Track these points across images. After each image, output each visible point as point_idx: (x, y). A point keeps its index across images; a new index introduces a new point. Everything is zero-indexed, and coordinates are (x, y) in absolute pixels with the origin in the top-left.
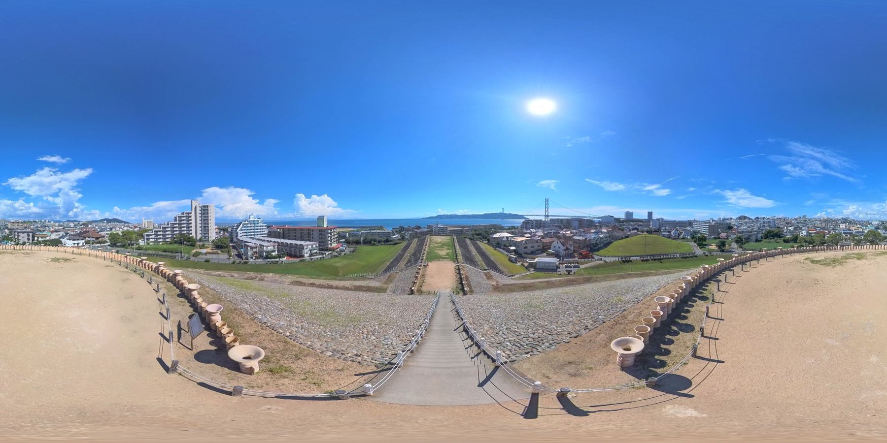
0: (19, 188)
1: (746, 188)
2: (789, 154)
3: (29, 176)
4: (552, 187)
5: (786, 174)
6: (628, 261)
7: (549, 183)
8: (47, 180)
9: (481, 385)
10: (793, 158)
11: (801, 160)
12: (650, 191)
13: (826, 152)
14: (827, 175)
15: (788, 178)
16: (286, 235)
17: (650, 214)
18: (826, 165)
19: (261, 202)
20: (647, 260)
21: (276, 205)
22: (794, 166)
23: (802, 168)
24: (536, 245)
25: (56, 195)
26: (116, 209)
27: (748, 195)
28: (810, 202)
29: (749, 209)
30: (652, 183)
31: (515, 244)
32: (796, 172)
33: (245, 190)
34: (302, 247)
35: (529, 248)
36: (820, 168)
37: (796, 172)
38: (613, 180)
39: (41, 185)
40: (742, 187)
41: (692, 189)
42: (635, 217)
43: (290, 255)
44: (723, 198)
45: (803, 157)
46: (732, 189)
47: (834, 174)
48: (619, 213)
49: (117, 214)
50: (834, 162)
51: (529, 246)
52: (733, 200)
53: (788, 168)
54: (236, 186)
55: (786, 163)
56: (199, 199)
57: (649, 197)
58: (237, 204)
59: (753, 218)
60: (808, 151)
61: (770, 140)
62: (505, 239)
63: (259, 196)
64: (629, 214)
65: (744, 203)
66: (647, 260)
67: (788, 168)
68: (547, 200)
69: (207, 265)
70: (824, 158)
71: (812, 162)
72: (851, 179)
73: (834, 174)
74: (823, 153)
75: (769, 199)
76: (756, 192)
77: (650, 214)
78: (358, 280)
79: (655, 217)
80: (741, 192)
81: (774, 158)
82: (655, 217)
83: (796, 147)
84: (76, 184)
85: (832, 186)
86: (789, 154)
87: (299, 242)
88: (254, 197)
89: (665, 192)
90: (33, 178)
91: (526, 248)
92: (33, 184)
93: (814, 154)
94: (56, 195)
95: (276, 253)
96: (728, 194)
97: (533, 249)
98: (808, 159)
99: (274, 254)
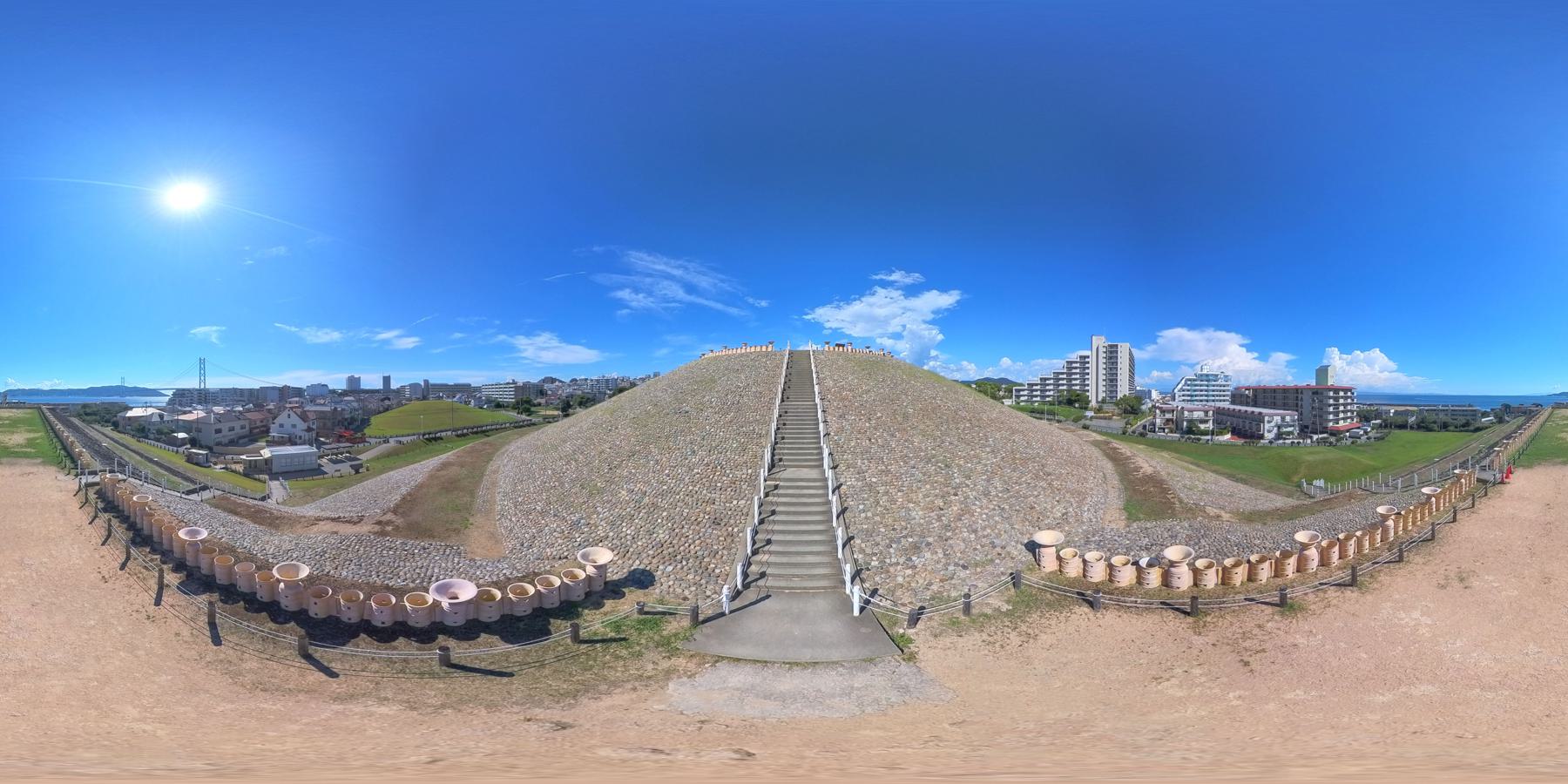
0: (834, 325)
1: (552, 330)
2: (627, 271)
3: (848, 301)
5: (622, 304)
6: (436, 439)
7: (209, 332)
8: (881, 312)
9: (123, 567)
11: (648, 280)
12: (386, 342)
13: (690, 266)
14: (691, 305)
15: (625, 311)
16: (1260, 399)
17: (387, 380)
18: (690, 289)
19: (1263, 357)
20: (464, 435)
22: (636, 290)
23: (650, 293)
24: (237, 425)
25: (897, 336)
26: (1006, 361)
27: (555, 343)
28: (664, 351)
29: (556, 366)
30: (389, 328)
31: (187, 426)
32: (639, 301)
33: (1233, 335)
34: (1260, 419)
35: (225, 432)
36: (681, 294)
37: (639, 301)
39: (871, 319)
40: (545, 330)
41: (458, 335)
42: (365, 385)
43: (1236, 432)
44: (512, 348)
45: (650, 275)
46: (529, 333)
47: (706, 302)
48: (337, 382)
49: (1006, 370)
50: (704, 282)
51: (225, 427)
52: (529, 352)
53: (625, 294)
54: (1219, 328)
55: (621, 287)
56: (1151, 348)
59: (567, 380)
62: (156, 419)
63: (1259, 346)
64: (353, 381)
65: (548, 356)
66: (464, 435)
67: (625, 294)
68: (202, 362)
69: (1161, 445)
71: (666, 283)
72: (734, 311)
73: (706, 302)
74: (686, 269)
75: (590, 347)
76: (568, 336)
77: (387, 380)
79: (394, 385)
80: (544, 339)
81: (601, 278)
82: (394, 385)
83: (639, 259)
84: (932, 316)
86: (627, 271)
87: (1257, 410)
88: (1249, 348)
89: (410, 342)
90: (857, 307)
91: (218, 431)
92: (858, 318)
93: (669, 270)
94: (897, 336)
95: (1210, 425)
96: (521, 341)
97: (232, 435)
98: (659, 278)
99: (1202, 427)
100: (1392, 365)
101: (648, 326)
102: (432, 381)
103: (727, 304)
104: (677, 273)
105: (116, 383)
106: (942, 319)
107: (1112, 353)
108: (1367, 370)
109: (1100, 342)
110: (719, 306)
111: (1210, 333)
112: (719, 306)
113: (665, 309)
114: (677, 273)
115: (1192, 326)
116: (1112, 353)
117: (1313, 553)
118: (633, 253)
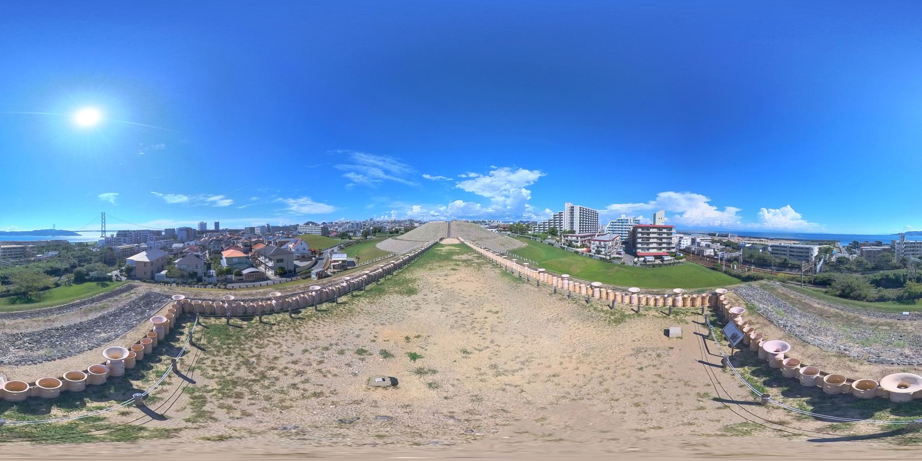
4: (112, 201)
5: (349, 181)
7: (109, 196)
10: (358, 167)
11: (365, 168)
12: (214, 202)
13: (388, 160)
14: (387, 181)
15: (351, 185)
17: (217, 224)
18: (387, 172)
19: (721, 209)
21: (737, 213)
22: (358, 173)
23: (365, 174)
28: (371, 206)
30: (217, 194)
32: (358, 178)
33: (700, 196)
36: (381, 174)
37: (358, 178)
38: (177, 193)
41: (254, 198)
45: (365, 165)
46: (295, 197)
48: (194, 225)
50: (395, 168)
53: (351, 175)
54: (693, 192)
55: (350, 171)
57: (213, 209)
58: (696, 212)
60: (371, 159)
61: (339, 151)
63: (718, 203)
64: (203, 225)
65: (305, 210)
67: (351, 175)
68: (103, 215)
70: (386, 166)
72: (411, 183)
75: (328, 204)
76: (317, 199)
77: (217, 224)
78: (70, 313)
80: (302, 200)
81: (339, 167)
83: (360, 157)
85: (391, 189)
88: (710, 204)
89: (227, 203)
96: (291, 201)
98: (372, 167)
100: (798, 215)
101: (362, 192)
102: (271, 225)
103: (407, 180)
104: (381, 164)
105: (49, 227)
106: (534, 187)
107: (572, 209)
108: (783, 219)
109: (568, 206)
110: (402, 181)
111: (689, 195)
112: (402, 181)
113: (373, 183)
114: (381, 164)
115: (676, 192)
116: (572, 209)
117: (680, 298)
118: (357, 154)
